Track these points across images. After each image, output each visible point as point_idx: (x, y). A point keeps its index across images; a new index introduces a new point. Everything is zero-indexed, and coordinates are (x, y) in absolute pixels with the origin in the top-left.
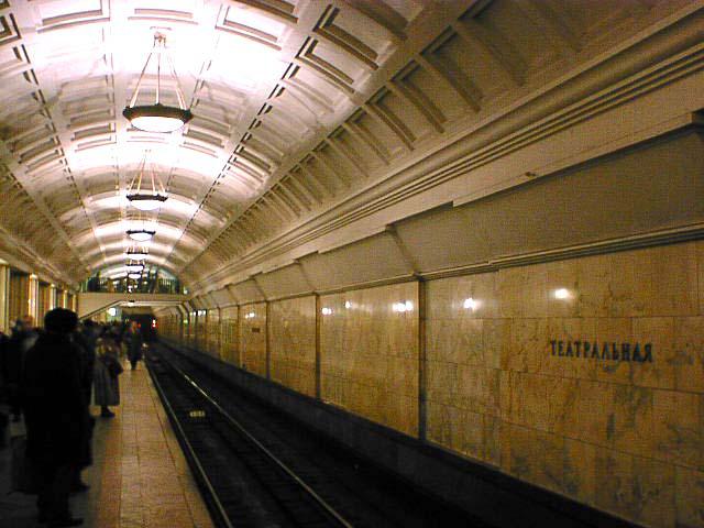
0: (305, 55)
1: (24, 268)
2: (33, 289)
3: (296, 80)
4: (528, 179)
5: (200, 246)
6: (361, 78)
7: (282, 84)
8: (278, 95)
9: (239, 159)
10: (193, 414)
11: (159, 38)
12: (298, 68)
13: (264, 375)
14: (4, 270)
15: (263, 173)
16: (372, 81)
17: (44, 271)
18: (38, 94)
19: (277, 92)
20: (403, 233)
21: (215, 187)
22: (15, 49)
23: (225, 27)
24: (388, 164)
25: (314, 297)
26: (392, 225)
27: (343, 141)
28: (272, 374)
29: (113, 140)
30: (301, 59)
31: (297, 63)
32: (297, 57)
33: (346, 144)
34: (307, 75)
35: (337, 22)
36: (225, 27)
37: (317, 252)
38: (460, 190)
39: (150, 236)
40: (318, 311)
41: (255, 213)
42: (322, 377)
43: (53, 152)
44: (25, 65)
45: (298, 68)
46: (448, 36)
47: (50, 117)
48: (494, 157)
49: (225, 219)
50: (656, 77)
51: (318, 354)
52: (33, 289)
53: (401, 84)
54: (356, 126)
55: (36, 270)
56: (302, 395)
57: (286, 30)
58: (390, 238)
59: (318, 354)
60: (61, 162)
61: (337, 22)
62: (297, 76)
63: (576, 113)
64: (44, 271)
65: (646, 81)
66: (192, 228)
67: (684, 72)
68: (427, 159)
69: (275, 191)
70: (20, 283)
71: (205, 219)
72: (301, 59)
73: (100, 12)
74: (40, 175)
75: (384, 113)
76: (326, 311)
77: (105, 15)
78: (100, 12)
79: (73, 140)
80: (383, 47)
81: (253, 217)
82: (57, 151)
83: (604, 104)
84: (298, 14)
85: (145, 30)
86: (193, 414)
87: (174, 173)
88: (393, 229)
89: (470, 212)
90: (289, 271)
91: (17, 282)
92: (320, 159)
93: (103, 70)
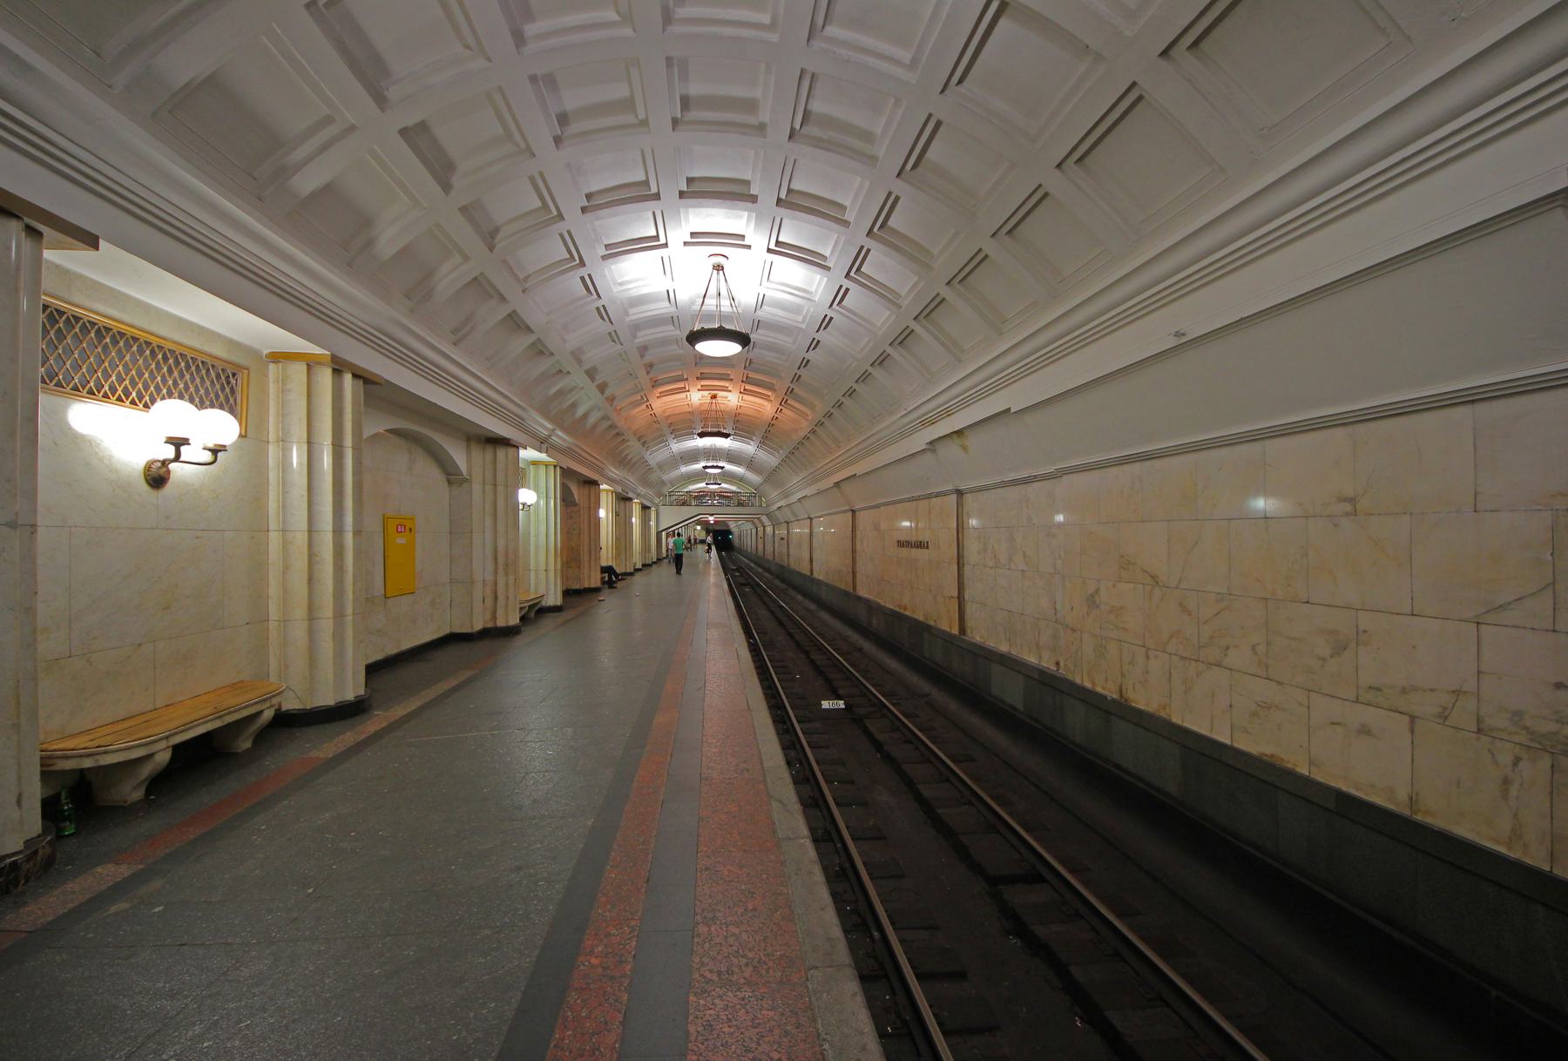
1: (648, 504)
2: (636, 509)
3: (844, 308)
5: (769, 459)
8: (825, 329)
10: (826, 704)
11: (719, 268)
13: (949, 625)
17: (644, 497)
18: (613, 334)
20: (842, 485)
22: (582, 279)
26: (931, 443)
28: (769, 549)
30: (834, 310)
31: (847, 284)
32: (847, 276)
37: (855, 475)
44: (595, 300)
45: (847, 290)
47: (622, 344)
48: (1220, 273)
49: (781, 452)
52: (636, 509)
53: (924, 321)
54: (900, 348)
55: (638, 495)
58: (835, 490)
63: (1022, 370)
64: (644, 497)
65: (1035, 362)
66: (767, 433)
67: (1243, 261)
72: (834, 310)
73: (657, 238)
75: (931, 328)
77: (662, 241)
78: (657, 238)
84: (850, 216)
85: (702, 256)
86: (826, 704)
87: (739, 411)
88: (837, 484)
91: (586, 493)
92: (827, 422)
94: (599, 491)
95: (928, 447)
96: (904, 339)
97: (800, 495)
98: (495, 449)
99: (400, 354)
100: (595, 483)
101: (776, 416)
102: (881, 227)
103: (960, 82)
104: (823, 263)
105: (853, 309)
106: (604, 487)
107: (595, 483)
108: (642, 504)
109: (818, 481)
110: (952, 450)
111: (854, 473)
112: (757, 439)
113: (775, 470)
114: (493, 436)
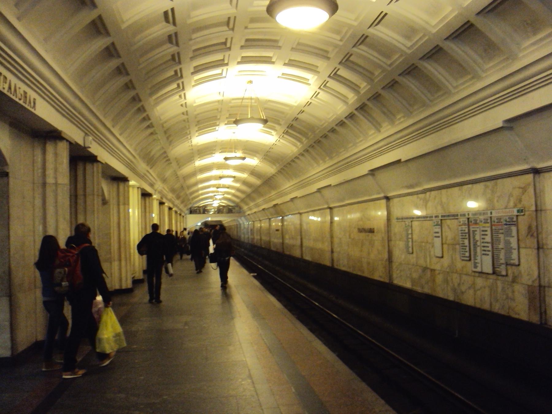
0: (323, 87)
1: (149, 189)
4: (344, 181)
6: (365, 87)
7: (310, 101)
8: (308, 106)
9: (290, 131)
12: (319, 93)
14: (136, 190)
15: (299, 144)
16: (357, 100)
19: (301, 112)
21: (270, 150)
23: (283, 76)
24: (380, 131)
25: (268, 220)
26: (319, 189)
27: (365, 111)
29: (217, 129)
30: (313, 100)
31: (319, 91)
33: (369, 115)
34: (323, 95)
35: (338, 73)
36: (283, 76)
37: (297, 197)
38: (333, 180)
39: (233, 179)
40: (332, 219)
41: (296, 160)
42: (304, 249)
43: (172, 73)
45: (319, 93)
46: (437, 49)
50: (425, 132)
51: (301, 239)
55: (141, 177)
56: (291, 258)
57: (313, 77)
59: (301, 239)
60: (178, 85)
61: (338, 73)
62: (318, 96)
68: (323, 170)
69: (280, 172)
70: (118, 188)
71: (244, 188)
72: (313, 100)
74: (187, 169)
76: (336, 219)
79: (197, 131)
80: (364, 86)
81: (296, 163)
82: (176, 72)
83: (456, 120)
84: (331, 55)
89: (410, 165)
90: (289, 204)
91: (115, 189)
93: (220, 98)
94: (128, 186)
95: (506, 125)
96: (351, 116)
97: (293, 195)
98: (56, 144)
99: (71, 114)
100: (124, 179)
101: (276, 143)
102: (346, 60)
103: (376, 25)
104: (307, 82)
105: (323, 99)
106: (132, 183)
107: (124, 179)
108: (143, 190)
109: (340, 171)
110: (290, 204)
111: (329, 184)
112: (281, 129)
113: (244, 199)
114: (146, 193)
